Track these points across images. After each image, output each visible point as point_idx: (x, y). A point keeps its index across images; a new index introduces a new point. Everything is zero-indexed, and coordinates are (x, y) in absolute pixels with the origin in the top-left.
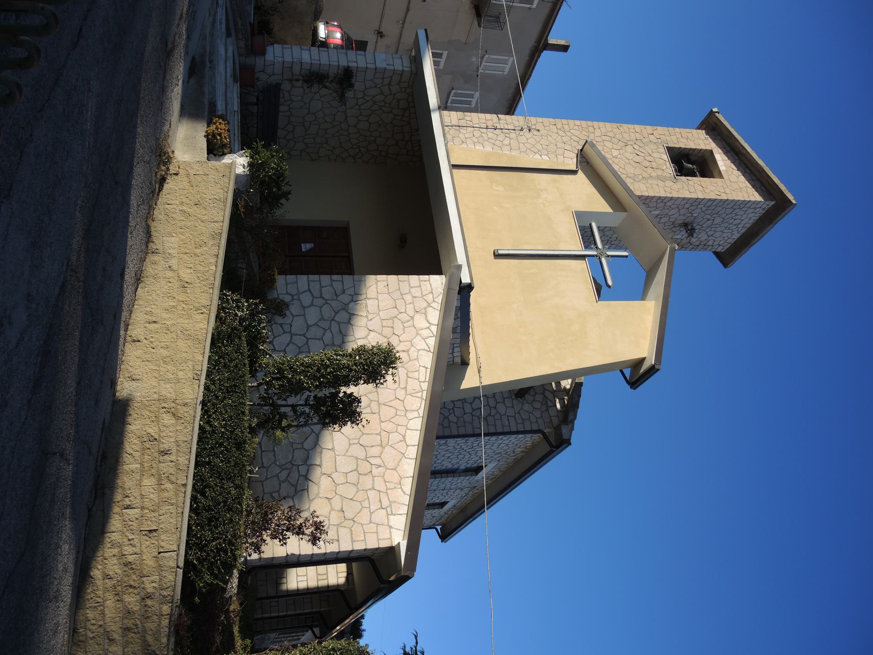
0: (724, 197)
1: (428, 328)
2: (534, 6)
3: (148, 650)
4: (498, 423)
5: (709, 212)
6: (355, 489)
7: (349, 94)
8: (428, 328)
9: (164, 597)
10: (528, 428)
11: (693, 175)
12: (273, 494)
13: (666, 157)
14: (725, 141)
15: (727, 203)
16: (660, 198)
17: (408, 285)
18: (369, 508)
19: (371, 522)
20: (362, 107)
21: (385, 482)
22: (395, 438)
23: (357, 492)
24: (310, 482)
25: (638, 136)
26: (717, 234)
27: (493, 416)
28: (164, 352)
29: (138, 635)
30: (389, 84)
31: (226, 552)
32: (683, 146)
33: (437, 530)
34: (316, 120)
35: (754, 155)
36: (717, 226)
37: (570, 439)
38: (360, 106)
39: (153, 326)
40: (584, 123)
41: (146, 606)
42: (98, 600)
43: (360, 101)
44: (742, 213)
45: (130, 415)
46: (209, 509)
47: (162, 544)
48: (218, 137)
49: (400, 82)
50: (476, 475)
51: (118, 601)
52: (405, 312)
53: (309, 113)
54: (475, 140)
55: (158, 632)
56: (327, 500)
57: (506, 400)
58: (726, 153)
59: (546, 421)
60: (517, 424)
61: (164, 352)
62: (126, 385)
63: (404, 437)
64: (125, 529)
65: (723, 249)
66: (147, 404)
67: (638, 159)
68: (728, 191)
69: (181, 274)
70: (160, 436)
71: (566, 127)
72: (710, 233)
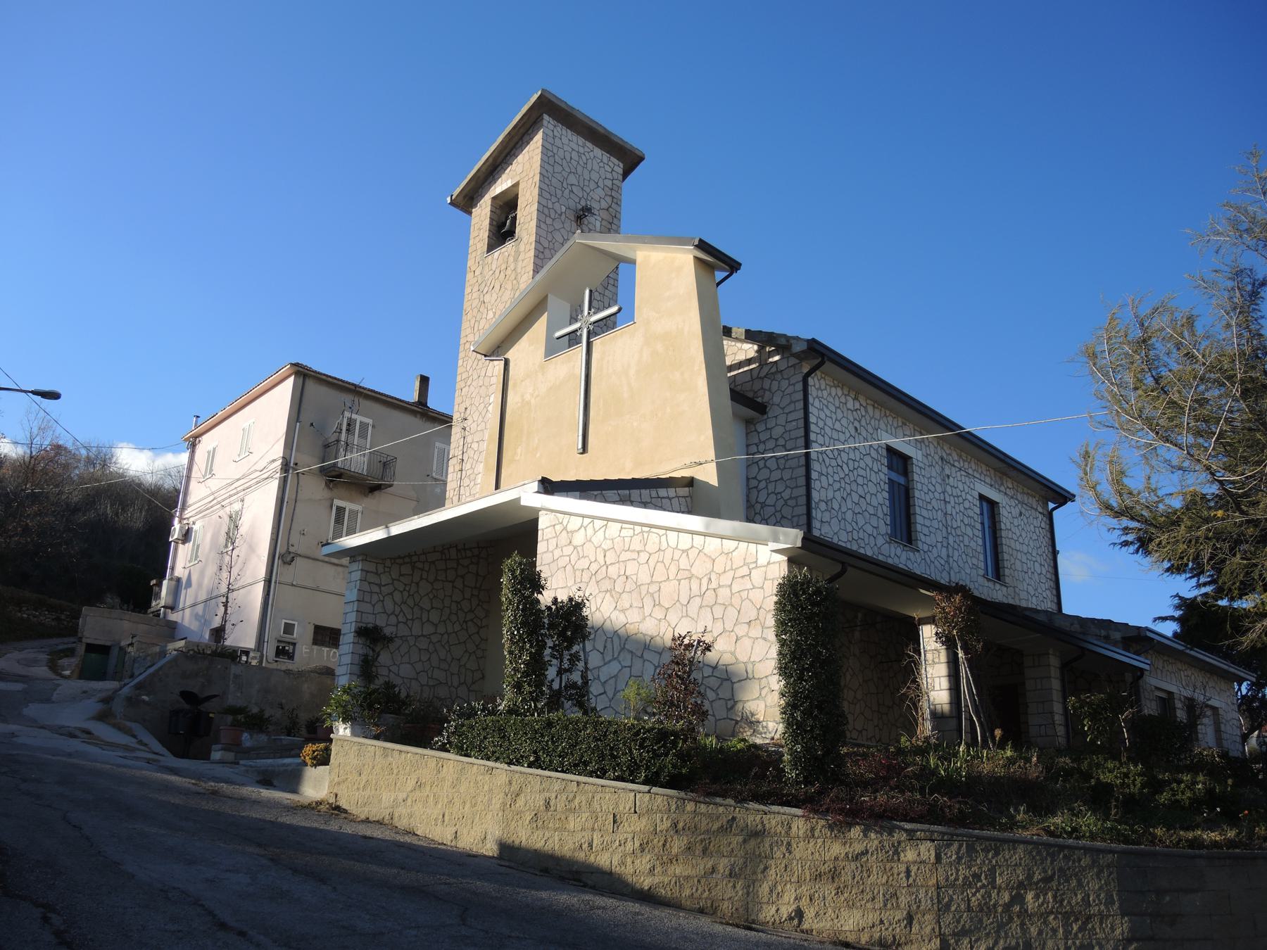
0: (537, 178)
1: (585, 528)
2: (370, 421)
3: (727, 829)
4: (794, 434)
5: (559, 193)
6: (730, 608)
7: (388, 631)
8: (585, 528)
9: (677, 807)
10: (800, 396)
11: (515, 218)
12: (729, 707)
13: (496, 253)
14: (483, 183)
15: (545, 174)
16: (536, 256)
17: (371, 570)
18: (748, 590)
19: (762, 588)
20: (410, 617)
21: (725, 572)
22: (684, 563)
23: (732, 605)
24: (720, 663)
25: (476, 289)
26: (595, 176)
27: (786, 441)
28: (468, 805)
29: (713, 839)
30: (380, 585)
31: (644, 740)
32: (487, 234)
33: (1054, 509)
34: (427, 672)
35: (492, 148)
36: (581, 179)
37: (808, 341)
38: (407, 619)
39: (447, 818)
40: (461, 355)
41: (684, 829)
42: (673, 882)
43: (401, 618)
44: (561, 153)
45: (513, 842)
46: (602, 757)
47: (627, 808)
48: (316, 753)
49: (376, 573)
50: (911, 458)
51: (677, 860)
52: (569, 556)
53: (417, 679)
54: (472, 483)
55: (710, 816)
56: (738, 642)
57: (768, 426)
58: (494, 181)
59: (792, 373)
60: (795, 410)
61: (468, 805)
62: (488, 846)
63: (683, 551)
64: (611, 849)
65: (619, 166)
66: (505, 824)
67: (497, 287)
68: (531, 175)
69: (409, 789)
70: (533, 810)
71: (464, 376)
72: (593, 185)
